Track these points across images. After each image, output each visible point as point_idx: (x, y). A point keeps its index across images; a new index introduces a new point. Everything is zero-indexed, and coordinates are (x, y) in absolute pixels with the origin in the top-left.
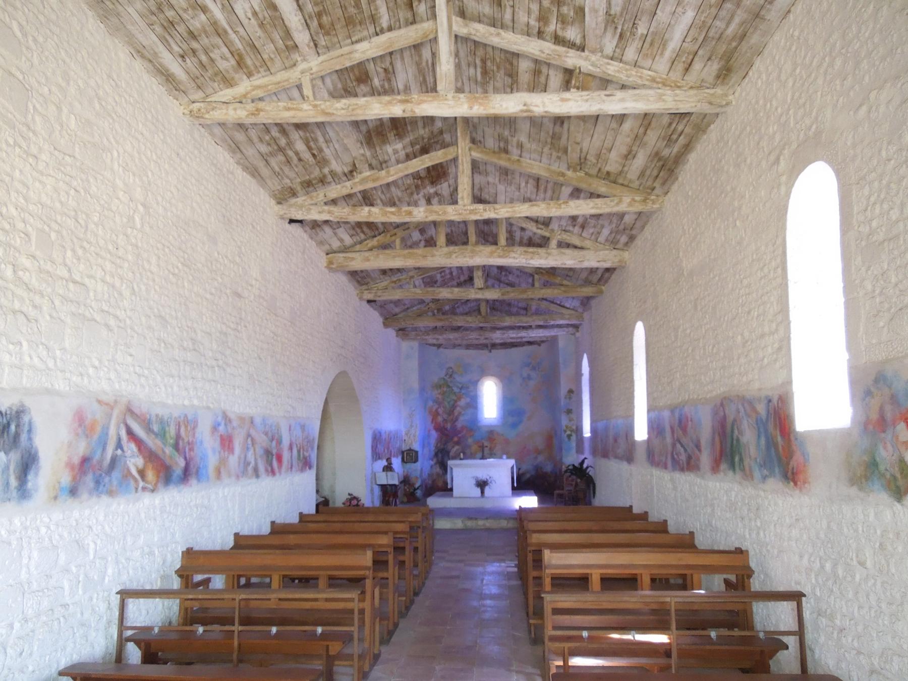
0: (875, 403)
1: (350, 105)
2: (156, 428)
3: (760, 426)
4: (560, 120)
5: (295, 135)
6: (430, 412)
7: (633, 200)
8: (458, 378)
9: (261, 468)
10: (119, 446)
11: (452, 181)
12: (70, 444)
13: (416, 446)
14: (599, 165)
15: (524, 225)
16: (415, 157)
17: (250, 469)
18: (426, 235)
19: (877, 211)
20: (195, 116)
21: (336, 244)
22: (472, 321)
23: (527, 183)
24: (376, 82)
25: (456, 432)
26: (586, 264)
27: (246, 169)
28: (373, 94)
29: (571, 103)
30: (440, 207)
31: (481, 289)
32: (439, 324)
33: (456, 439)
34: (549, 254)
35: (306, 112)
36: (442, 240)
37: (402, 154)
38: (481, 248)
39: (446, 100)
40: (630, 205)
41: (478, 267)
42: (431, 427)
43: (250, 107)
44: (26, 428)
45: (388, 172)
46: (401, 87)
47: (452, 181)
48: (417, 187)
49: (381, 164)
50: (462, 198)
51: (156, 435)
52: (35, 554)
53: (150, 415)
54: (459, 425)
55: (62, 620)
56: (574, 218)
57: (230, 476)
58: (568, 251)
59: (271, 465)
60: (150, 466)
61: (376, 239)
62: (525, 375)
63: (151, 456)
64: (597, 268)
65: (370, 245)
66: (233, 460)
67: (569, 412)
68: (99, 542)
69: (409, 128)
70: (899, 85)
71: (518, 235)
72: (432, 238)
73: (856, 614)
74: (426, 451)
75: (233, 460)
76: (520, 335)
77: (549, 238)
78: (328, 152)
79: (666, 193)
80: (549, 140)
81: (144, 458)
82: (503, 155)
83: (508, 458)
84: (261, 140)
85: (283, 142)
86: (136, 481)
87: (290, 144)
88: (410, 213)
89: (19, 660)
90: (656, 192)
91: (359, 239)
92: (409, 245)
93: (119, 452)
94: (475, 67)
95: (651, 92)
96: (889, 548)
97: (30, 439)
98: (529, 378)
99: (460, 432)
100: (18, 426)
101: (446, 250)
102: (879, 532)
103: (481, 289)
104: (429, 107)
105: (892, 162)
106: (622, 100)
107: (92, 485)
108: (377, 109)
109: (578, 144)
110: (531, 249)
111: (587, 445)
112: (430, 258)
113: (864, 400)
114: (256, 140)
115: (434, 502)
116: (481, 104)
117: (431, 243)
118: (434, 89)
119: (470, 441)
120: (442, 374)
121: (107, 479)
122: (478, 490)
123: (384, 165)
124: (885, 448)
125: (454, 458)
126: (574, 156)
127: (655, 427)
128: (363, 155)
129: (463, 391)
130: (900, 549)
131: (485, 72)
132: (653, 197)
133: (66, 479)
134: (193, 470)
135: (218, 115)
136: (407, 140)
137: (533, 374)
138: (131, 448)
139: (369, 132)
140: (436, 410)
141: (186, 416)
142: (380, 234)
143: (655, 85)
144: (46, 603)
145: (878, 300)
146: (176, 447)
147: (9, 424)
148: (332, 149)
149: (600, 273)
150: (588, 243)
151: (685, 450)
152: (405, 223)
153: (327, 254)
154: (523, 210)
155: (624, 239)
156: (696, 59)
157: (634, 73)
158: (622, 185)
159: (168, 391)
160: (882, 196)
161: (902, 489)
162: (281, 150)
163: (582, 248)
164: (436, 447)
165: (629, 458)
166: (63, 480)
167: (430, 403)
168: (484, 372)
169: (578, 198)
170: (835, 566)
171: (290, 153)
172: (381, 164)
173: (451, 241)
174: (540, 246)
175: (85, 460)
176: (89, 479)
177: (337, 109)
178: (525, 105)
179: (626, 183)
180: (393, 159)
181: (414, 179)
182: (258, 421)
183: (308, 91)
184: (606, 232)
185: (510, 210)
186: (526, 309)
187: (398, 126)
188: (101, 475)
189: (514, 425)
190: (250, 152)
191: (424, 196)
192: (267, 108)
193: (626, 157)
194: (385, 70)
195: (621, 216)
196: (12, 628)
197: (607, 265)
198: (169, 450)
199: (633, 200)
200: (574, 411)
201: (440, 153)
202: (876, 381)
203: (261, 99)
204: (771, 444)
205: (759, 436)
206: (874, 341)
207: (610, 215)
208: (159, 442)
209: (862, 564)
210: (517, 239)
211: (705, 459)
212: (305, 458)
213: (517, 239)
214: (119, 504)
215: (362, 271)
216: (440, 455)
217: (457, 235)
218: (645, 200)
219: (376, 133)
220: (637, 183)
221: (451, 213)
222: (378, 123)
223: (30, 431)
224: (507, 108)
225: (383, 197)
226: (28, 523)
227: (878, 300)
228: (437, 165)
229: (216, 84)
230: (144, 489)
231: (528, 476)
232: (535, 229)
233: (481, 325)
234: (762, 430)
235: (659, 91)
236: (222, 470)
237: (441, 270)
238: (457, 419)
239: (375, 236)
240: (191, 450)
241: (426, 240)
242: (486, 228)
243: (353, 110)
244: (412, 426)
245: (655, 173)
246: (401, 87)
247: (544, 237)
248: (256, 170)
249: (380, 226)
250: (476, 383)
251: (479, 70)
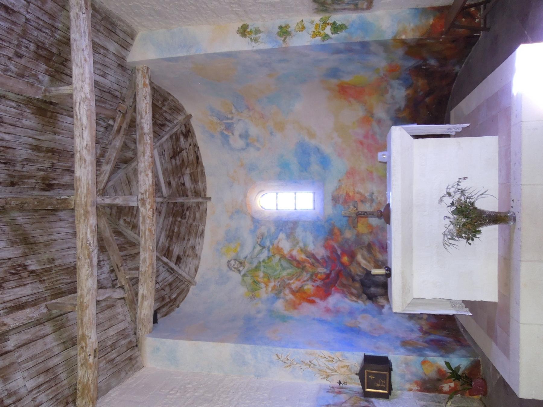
6: (294, 306)
8: (247, 251)
13: (355, 359)
25: (333, 258)
33: (345, 259)
42: (321, 304)
54: (321, 252)
62: (240, 143)
83: (384, 146)
98: (245, 136)
99: (333, 250)
119: (349, 234)
120: (236, 277)
122: (490, 233)
129: (268, 243)
137: (239, 128)
140: (293, 292)
164: (358, 297)
167: (279, 305)
168: (241, 210)
189: (325, 162)
216: (373, 290)
238: (313, 256)
244: (310, 364)
250: (256, 222)
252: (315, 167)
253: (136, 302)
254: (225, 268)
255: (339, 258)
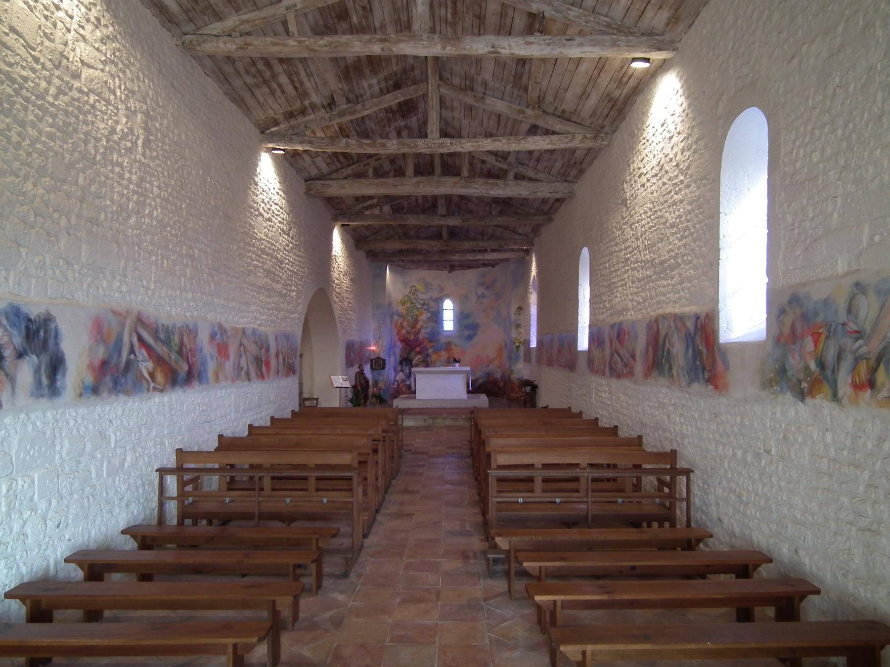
0: (788, 320)
1: (332, 43)
2: (162, 336)
3: (690, 339)
4: (522, 62)
5: (278, 68)
7: (585, 137)
8: (421, 296)
9: (253, 373)
10: (132, 351)
11: (420, 116)
12: (90, 349)
14: (555, 104)
15: (484, 158)
16: (388, 92)
17: (243, 372)
18: (395, 167)
19: (801, 154)
20: (188, 48)
21: (314, 172)
22: (436, 245)
23: (489, 118)
24: (355, 19)
26: (539, 195)
27: (233, 100)
28: (352, 33)
29: (535, 46)
30: (411, 140)
31: (444, 216)
32: (405, 247)
34: (506, 185)
35: (291, 47)
36: (410, 170)
37: (376, 89)
38: (446, 178)
39: (421, 40)
40: (582, 141)
41: (442, 196)
43: (239, 41)
44: (53, 334)
45: (364, 106)
46: (377, 25)
47: (420, 116)
48: (389, 120)
49: (357, 97)
50: (432, 132)
51: (162, 341)
52: (66, 443)
53: (157, 325)
55: (91, 498)
56: (531, 153)
57: (226, 379)
58: (524, 183)
59: (261, 370)
60: (159, 369)
61: (350, 168)
63: (159, 360)
64: (549, 199)
65: (345, 174)
66: (229, 365)
67: (518, 326)
68: (118, 433)
69: (384, 65)
70: (828, 40)
71: (479, 165)
72: (401, 168)
73: (760, 491)
74: (392, 359)
75: (229, 365)
76: (476, 258)
77: (506, 171)
78: (308, 85)
79: (615, 131)
80: (511, 79)
81: (154, 362)
82: (469, 92)
84: (247, 72)
85: (267, 74)
86: (148, 381)
87: (274, 76)
88: (384, 146)
89: (57, 530)
90: (605, 129)
91: (335, 168)
92: (379, 174)
93: (132, 356)
94: (446, 8)
95: (607, 38)
96: (791, 438)
97: (57, 344)
98: (483, 296)
100: (46, 332)
101: (414, 180)
102: (783, 426)
103: (444, 216)
104: (407, 48)
105: (817, 110)
106: (581, 45)
107: (111, 385)
108: (357, 47)
109: (538, 83)
110: (490, 181)
111: (534, 356)
112: (399, 187)
113: (779, 317)
114: (242, 72)
115: (400, 403)
116: (453, 45)
117: (400, 173)
118: (409, 27)
121: (123, 380)
123: (360, 99)
124: (793, 357)
125: (417, 366)
126: (533, 94)
127: (594, 338)
128: (341, 89)
130: (800, 439)
131: (455, 13)
132: (602, 135)
133: (89, 379)
134: (195, 373)
135: (209, 47)
136: (381, 76)
137: (487, 293)
138: (142, 353)
139: (347, 67)
141: (188, 325)
142: (354, 164)
143: (611, 31)
144: (77, 484)
145: (796, 232)
146: (180, 352)
147: (38, 331)
148: (313, 82)
149: (551, 202)
150: (541, 176)
151: (622, 360)
152: (377, 154)
153: (306, 181)
154: (488, 145)
155: (574, 172)
156: (649, 7)
157: (592, 19)
158: (575, 122)
159: (170, 301)
160: (807, 140)
161: (805, 391)
162: (265, 82)
163: (536, 180)
165: (571, 366)
166: (86, 381)
169: (535, 134)
170: (745, 453)
171: (274, 85)
172: (357, 97)
173: (418, 172)
174: (497, 177)
175: (104, 364)
176: (108, 379)
177: (320, 46)
178: (493, 47)
179: (579, 121)
180: (368, 94)
181: (386, 112)
182: (249, 332)
183: (292, 28)
184: (558, 165)
185: (475, 144)
186: (482, 234)
187: (374, 63)
188: (118, 377)
190: (237, 83)
191: (395, 129)
192: (256, 43)
193: (580, 98)
194: (364, 8)
195: (573, 151)
196: (50, 504)
197: (559, 196)
198: (174, 356)
199: (585, 137)
200: (521, 325)
201: (412, 88)
202: (790, 302)
203: (248, 34)
204: (697, 354)
205: (687, 348)
206: (791, 267)
207: (564, 150)
208: (165, 349)
209: (768, 452)
210: (478, 170)
211: (639, 367)
212: (289, 364)
213: (478, 170)
214: (134, 402)
215: (337, 198)
217: (425, 167)
218: (595, 137)
219: (352, 70)
220: (589, 121)
221: (422, 146)
222: (356, 59)
223: (56, 337)
224: (476, 50)
225: (358, 128)
226: (59, 416)
227: (796, 232)
228: (407, 100)
229: (206, 17)
230: (155, 389)
231: (481, 381)
232: (494, 162)
233: (443, 248)
234: (690, 342)
235: (614, 37)
236: (220, 374)
237: (408, 197)
238: (419, 331)
239: (350, 165)
240: (193, 355)
241: (395, 170)
242: (450, 161)
243: (336, 47)
244: (380, 338)
245: (606, 112)
246: (377, 25)
247: (501, 169)
248: (242, 100)
249: (354, 156)
251: (450, 10)
252: (467, 333)
253: (349, 171)
254: (411, 285)
255: (418, 346)
